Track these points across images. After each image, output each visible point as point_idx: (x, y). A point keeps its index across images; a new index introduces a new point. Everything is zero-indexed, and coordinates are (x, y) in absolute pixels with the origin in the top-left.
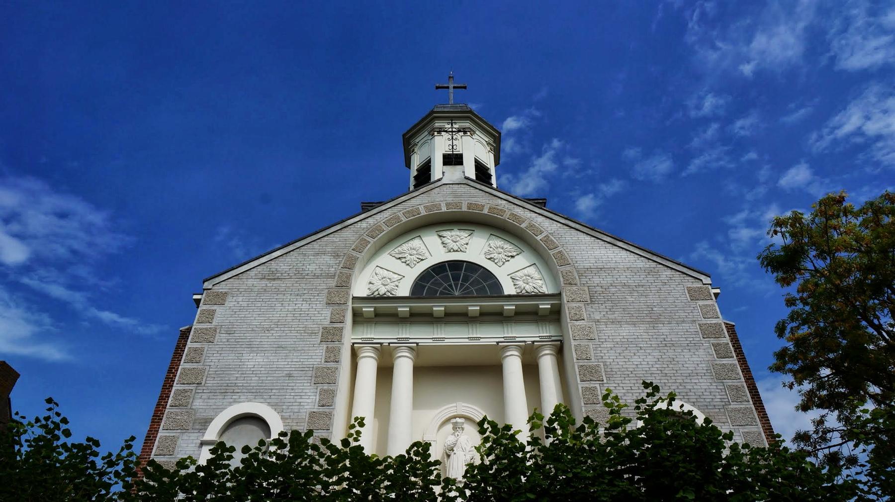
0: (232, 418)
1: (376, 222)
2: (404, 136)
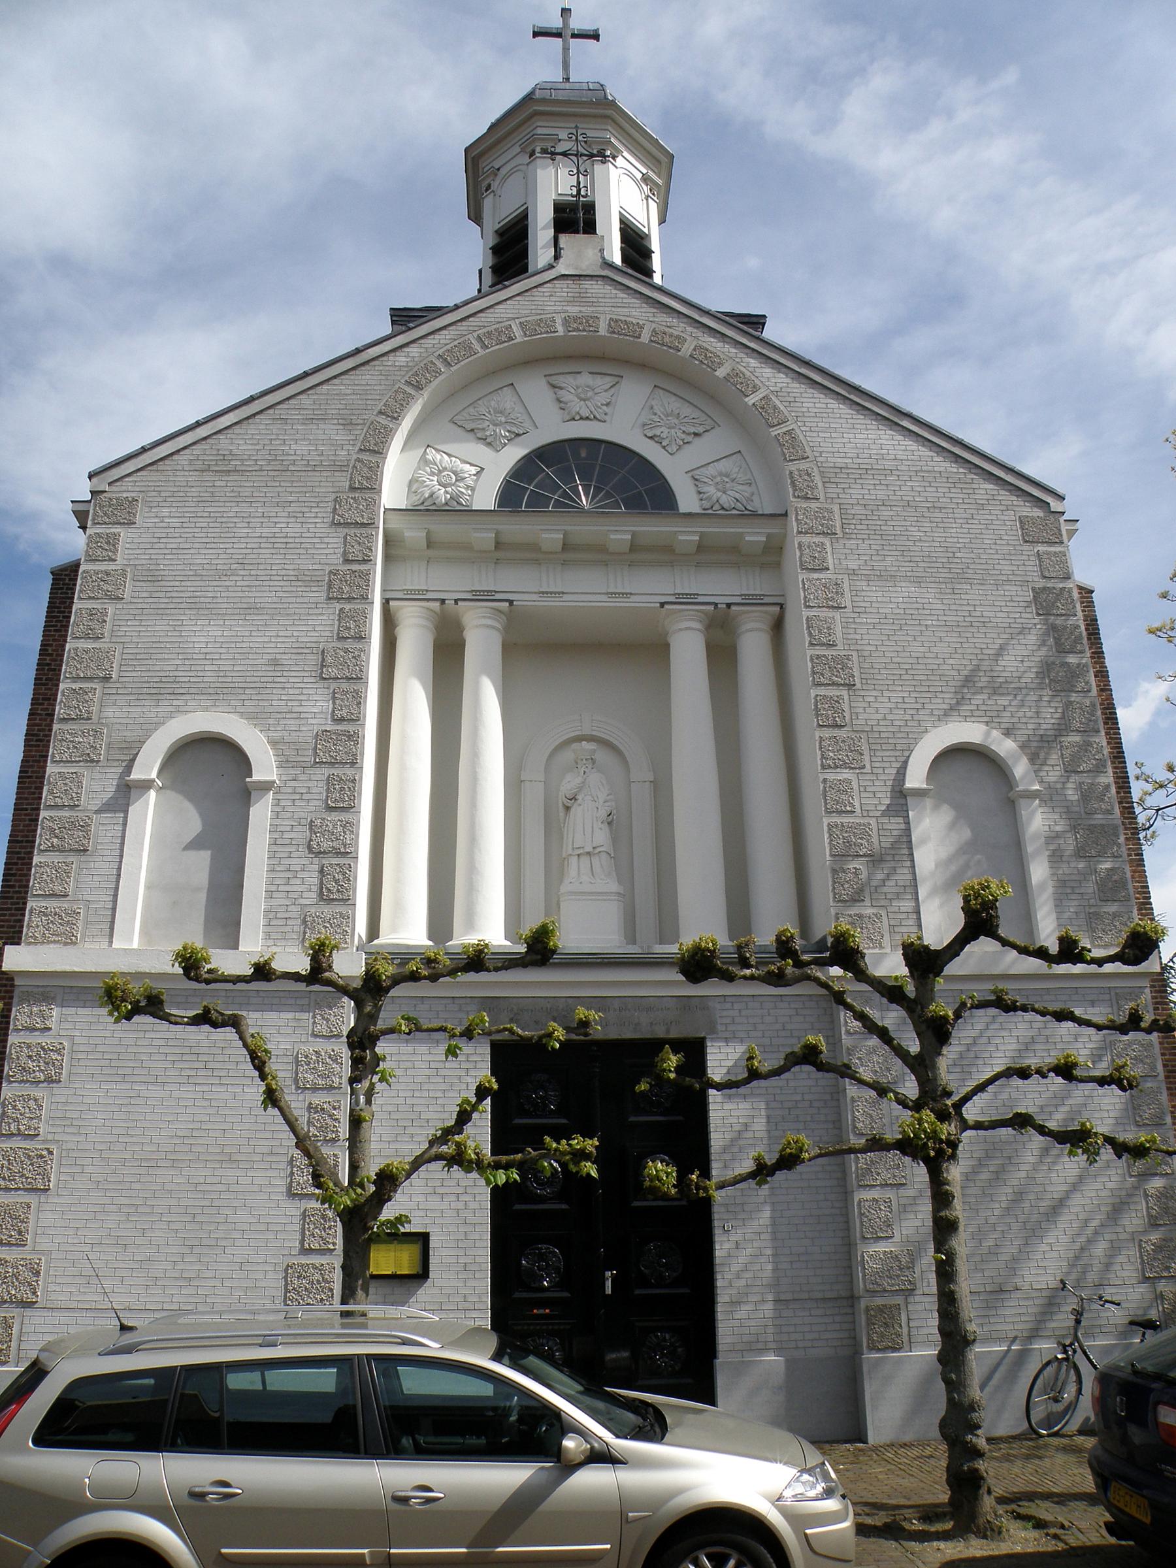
1: (425, 355)
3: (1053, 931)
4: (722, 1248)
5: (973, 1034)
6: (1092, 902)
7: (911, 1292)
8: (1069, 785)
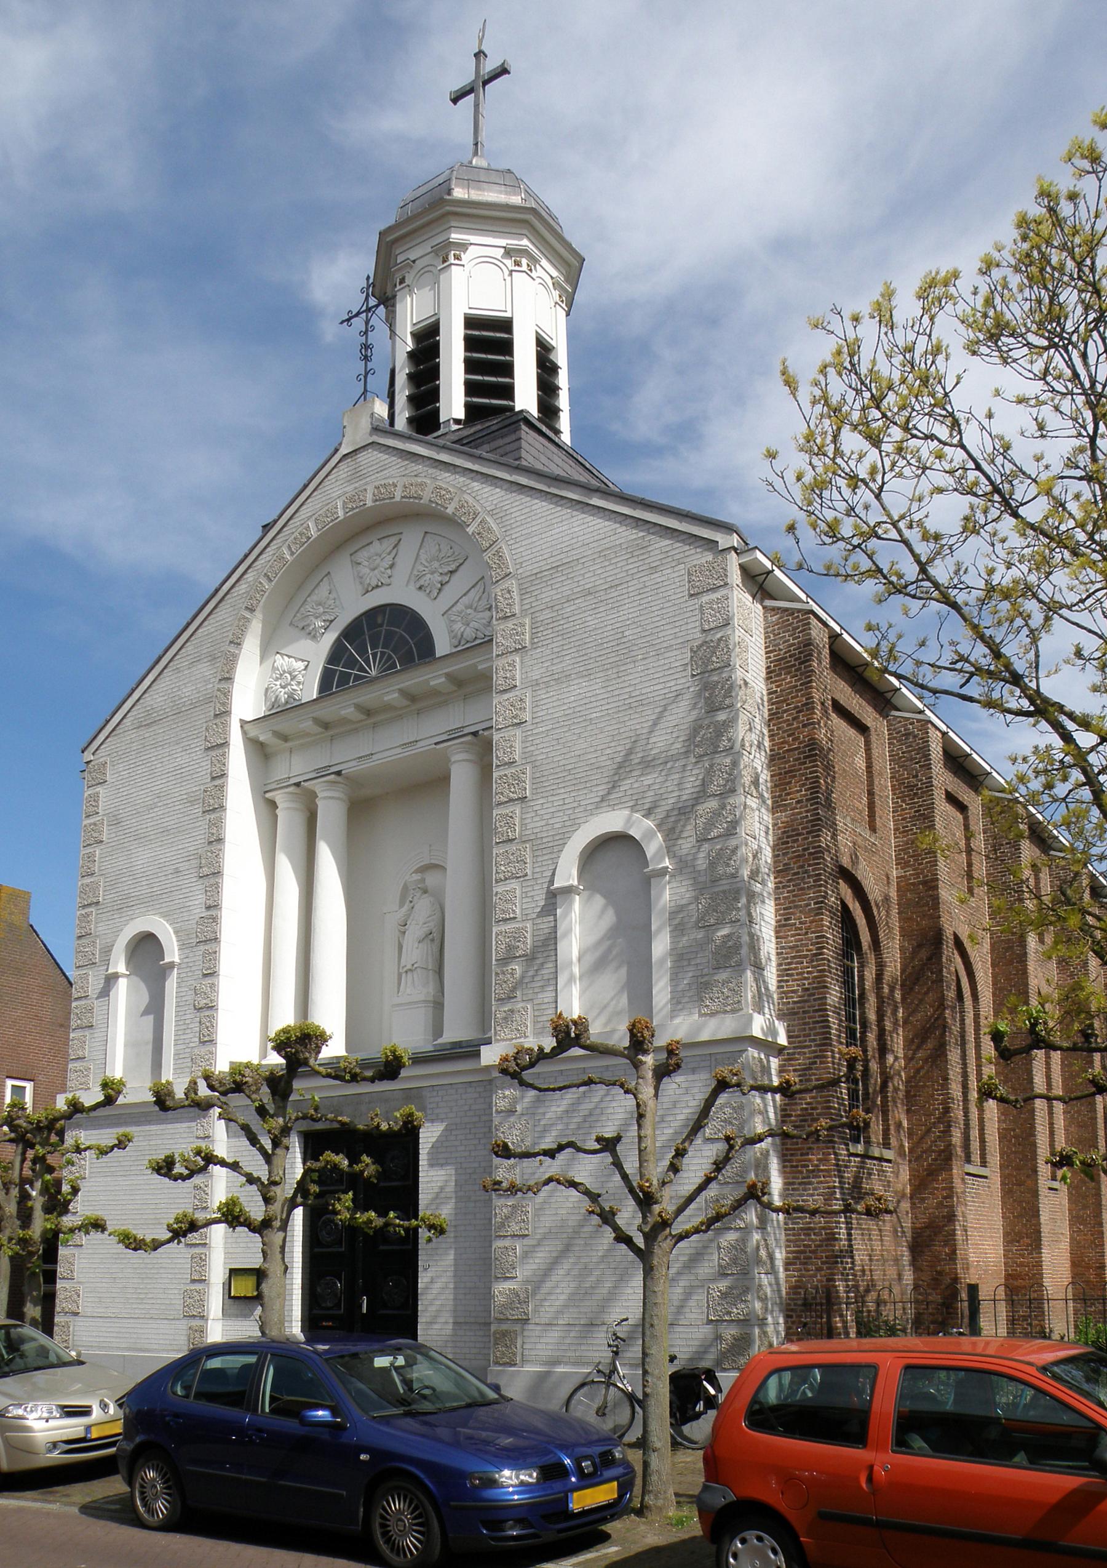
0: (107, 1479)
2: (381, 234)
3: (666, 1004)
4: (423, 1280)
5: (591, 1106)
6: (706, 971)
7: (526, 1321)
8: (702, 855)
